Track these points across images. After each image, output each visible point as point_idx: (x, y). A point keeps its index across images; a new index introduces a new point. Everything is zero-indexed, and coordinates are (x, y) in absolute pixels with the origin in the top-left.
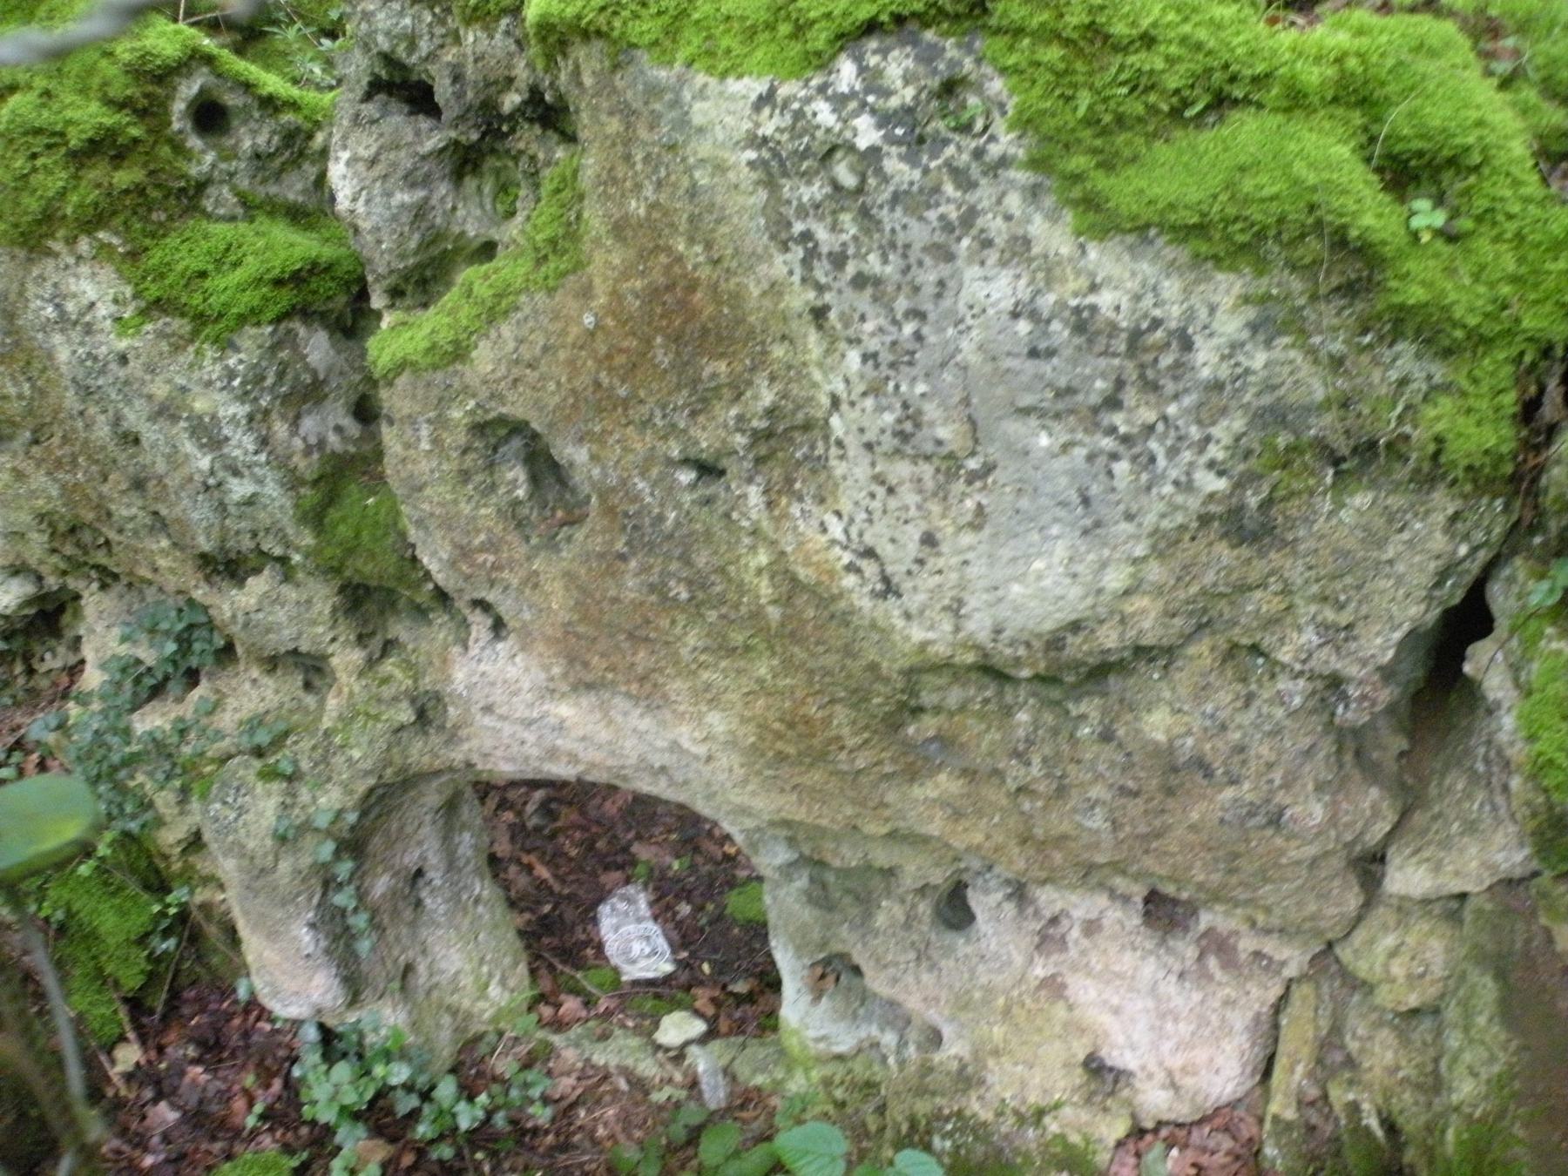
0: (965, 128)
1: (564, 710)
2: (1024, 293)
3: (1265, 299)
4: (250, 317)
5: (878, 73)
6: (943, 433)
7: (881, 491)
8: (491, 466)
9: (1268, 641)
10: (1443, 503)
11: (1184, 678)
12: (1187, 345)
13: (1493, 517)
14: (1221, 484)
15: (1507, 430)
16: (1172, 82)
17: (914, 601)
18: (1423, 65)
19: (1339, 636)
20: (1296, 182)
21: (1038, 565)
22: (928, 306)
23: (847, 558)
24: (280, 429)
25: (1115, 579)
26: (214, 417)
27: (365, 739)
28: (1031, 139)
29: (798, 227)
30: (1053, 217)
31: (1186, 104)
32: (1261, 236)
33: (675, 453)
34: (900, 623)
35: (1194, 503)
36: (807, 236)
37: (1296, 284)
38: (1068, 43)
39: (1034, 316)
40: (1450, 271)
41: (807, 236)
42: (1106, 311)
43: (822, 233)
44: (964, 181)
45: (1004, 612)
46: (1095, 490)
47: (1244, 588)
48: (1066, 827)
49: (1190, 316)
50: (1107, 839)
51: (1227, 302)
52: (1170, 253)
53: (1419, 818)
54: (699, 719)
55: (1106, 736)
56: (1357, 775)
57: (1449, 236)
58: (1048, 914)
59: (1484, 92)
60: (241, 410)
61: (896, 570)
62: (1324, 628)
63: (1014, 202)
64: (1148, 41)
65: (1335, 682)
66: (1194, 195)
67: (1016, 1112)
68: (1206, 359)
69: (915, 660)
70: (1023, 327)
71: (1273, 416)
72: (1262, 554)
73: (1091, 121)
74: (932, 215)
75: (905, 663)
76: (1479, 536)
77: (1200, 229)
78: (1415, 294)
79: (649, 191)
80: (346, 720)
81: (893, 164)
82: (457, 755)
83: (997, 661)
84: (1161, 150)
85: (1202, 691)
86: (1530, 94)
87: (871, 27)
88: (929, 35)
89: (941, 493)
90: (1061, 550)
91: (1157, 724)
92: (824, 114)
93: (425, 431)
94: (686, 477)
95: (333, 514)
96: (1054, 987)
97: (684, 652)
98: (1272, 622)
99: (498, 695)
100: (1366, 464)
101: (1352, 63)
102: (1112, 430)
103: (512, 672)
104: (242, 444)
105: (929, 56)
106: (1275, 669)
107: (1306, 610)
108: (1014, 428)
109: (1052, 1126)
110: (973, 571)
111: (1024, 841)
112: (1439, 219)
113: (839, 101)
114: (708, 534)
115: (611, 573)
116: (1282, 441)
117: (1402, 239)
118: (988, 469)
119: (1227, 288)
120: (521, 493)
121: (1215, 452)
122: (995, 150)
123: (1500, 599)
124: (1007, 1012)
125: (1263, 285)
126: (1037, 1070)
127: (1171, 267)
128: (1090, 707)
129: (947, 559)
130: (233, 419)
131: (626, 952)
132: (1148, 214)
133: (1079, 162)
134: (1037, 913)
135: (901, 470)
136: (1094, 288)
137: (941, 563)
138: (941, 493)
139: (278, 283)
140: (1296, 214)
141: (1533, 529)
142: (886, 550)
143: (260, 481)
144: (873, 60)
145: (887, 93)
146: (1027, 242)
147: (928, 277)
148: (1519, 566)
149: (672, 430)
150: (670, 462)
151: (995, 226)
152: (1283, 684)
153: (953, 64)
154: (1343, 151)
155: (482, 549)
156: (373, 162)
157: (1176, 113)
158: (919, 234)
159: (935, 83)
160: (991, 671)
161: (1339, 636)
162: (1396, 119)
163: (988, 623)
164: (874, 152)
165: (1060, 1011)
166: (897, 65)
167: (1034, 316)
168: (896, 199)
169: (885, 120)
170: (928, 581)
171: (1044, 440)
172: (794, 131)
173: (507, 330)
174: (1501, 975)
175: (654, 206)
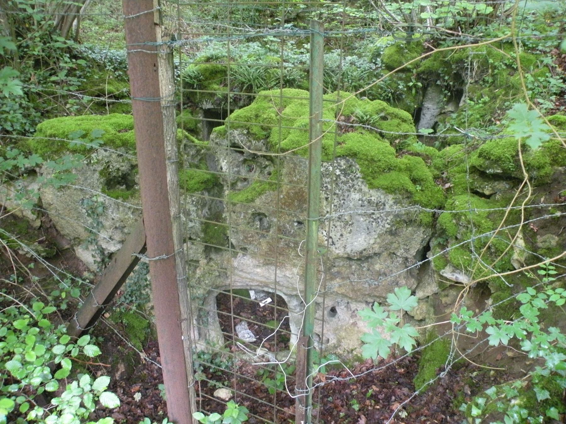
0: (352, 172)
1: (259, 270)
2: (361, 197)
3: (396, 198)
4: (197, 190)
5: (340, 163)
6: (346, 218)
7: (334, 227)
8: (254, 222)
9: (396, 252)
10: (422, 229)
11: (382, 259)
12: (385, 205)
13: (430, 231)
14: (389, 226)
15: (431, 218)
16: (383, 167)
17: (337, 246)
18: (419, 166)
19: (407, 251)
20: (401, 183)
21: (360, 239)
22: (346, 198)
23: (326, 238)
24: (200, 212)
25: (372, 241)
26: (189, 210)
27: (209, 279)
28: (362, 174)
29: (325, 185)
30: (365, 186)
31: (385, 170)
32: (396, 190)
33: (295, 220)
34: (334, 249)
35: (385, 229)
36: (326, 186)
37: (400, 197)
38: (368, 161)
39: (362, 200)
40: (422, 196)
41: (326, 186)
42: (373, 200)
43: (329, 187)
44: (353, 180)
45: (353, 247)
46: (369, 227)
47: (392, 243)
48: (361, 287)
49: (385, 201)
50: (368, 288)
51: (390, 199)
52: (382, 192)
53: (421, 284)
54: (291, 270)
55: (369, 270)
56: (410, 277)
57: (422, 190)
58: (353, 310)
59: (426, 170)
60: (195, 208)
61: (335, 240)
62: (405, 249)
63: (360, 183)
64: (379, 161)
65: (406, 259)
66: (386, 183)
67: (348, 351)
68: (387, 208)
69: (336, 256)
70: (360, 202)
71: (397, 216)
72: (395, 237)
73: (371, 172)
74: (348, 185)
75: (334, 257)
76: (427, 234)
77: (387, 189)
78: (417, 199)
79: (298, 177)
80: (203, 275)
81: (342, 177)
82: (228, 282)
83: (351, 256)
84: (381, 177)
85: (385, 261)
86: (433, 169)
87: (339, 156)
88: (347, 158)
89: (345, 227)
90: (363, 237)
91: (377, 267)
92: (331, 168)
93: (243, 215)
94: (296, 224)
95: (208, 230)
96: (355, 324)
97: (291, 257)
98: (397, 249)
99: (245, 267)
100: (410, 223)
101: (408, 165)
102: (373, 218)
103: (248, 262)
104: (193, 215)
105: (348, 161)
106: (397, 256)
107: (402, 246)
108: (357, 217)
109: (355, 353)
110: (348, 240)
111: (352, 291)
112: (420, 188)
113: (334, 167)
114: (299, 235)
115: (278, 242)
116: (398, 219)
117: (415, 191)
118: (353, 223)
119: (390, 197)
120: (258, 226)
121: (388, 221)
122: (357, 176)
123: (431, 245)
124: (345, 329)
125: (396, 196)
126: (352, 341)
127: (382, 194)
128: (366, 265)
129: (344, 238)
130: (193, 211)
131: (244, 337)
132: (379, 186)
133: (369, 178)
134: (351, 310)
135: (338, 223)
136: (371, 196)
137: (343, 239)
138: (345, 227)
139: (202, 183)
140: (401, 187)
141: (436, 233)
142: (333, 237)
143: (195, 223)
144: (339, 161)
145: (341, 166)
146: (361, 189)
147: (346, 194)
148: (433, 239)
149: (296, 216)
150: (294, 221)
151: (357, 187)
152: (398, 259)
153: (351, 163)
154: (407, 178)
155: (250, 237)
156: (231, 162)
157: (383, 171)
158: (345, 188)
159: (349, 165)
160: (349, 258)
161: (407, 251)
162: (414, 173)
163: (350, 249)
164: (339, 175)
165: (356, 329)
166: (343, 162)
167: (362, 200)
168: (342, 182)
169: (341, 171)
170: (340, 242)
171: (362, 219)
172: (326, 171)
173: (263, 197)
174: (434, 308)
175: (298, 179)
